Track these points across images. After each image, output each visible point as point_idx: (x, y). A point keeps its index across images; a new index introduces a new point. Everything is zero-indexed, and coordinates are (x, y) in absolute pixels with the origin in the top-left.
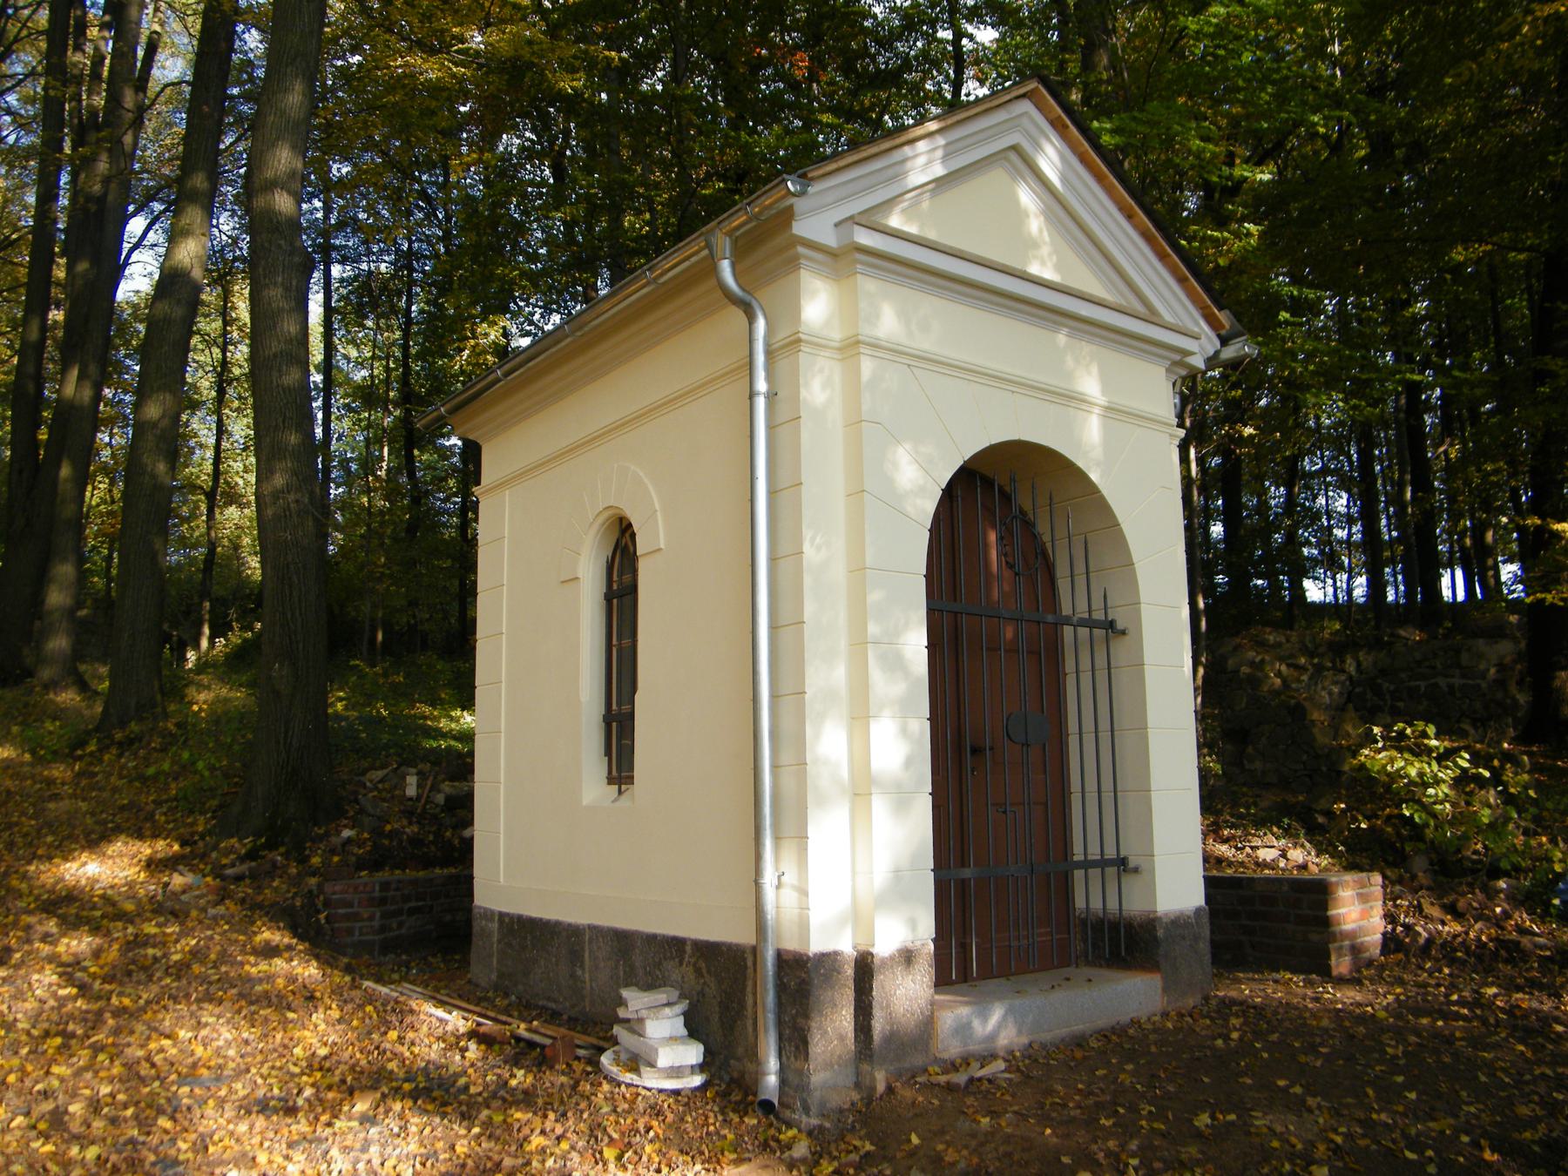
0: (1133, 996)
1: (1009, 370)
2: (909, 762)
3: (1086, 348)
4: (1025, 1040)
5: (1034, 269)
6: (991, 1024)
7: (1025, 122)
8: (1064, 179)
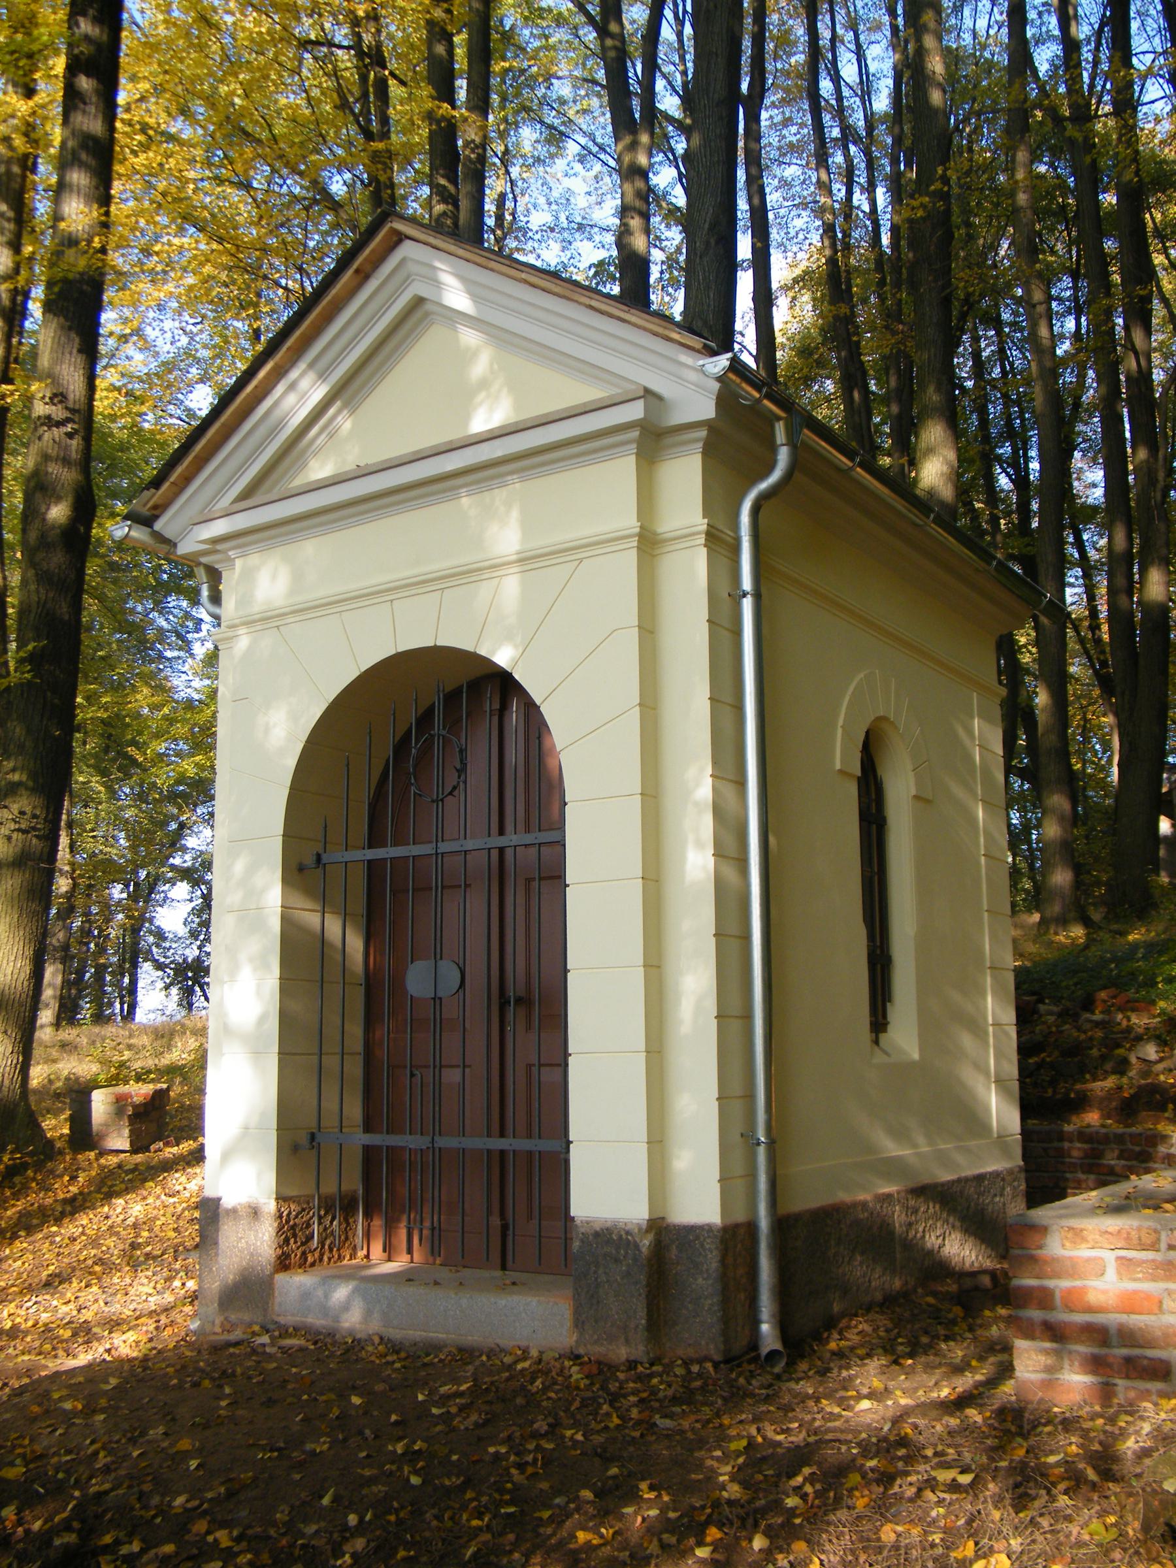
0: (530, 1319)
1: (373, 582)
2: (262, 1019)
3: (499, 495)
4: (375, 1326)
5: (482, 421)
6: (359, 1292)
7: (411, 267)
8: (474, 297)
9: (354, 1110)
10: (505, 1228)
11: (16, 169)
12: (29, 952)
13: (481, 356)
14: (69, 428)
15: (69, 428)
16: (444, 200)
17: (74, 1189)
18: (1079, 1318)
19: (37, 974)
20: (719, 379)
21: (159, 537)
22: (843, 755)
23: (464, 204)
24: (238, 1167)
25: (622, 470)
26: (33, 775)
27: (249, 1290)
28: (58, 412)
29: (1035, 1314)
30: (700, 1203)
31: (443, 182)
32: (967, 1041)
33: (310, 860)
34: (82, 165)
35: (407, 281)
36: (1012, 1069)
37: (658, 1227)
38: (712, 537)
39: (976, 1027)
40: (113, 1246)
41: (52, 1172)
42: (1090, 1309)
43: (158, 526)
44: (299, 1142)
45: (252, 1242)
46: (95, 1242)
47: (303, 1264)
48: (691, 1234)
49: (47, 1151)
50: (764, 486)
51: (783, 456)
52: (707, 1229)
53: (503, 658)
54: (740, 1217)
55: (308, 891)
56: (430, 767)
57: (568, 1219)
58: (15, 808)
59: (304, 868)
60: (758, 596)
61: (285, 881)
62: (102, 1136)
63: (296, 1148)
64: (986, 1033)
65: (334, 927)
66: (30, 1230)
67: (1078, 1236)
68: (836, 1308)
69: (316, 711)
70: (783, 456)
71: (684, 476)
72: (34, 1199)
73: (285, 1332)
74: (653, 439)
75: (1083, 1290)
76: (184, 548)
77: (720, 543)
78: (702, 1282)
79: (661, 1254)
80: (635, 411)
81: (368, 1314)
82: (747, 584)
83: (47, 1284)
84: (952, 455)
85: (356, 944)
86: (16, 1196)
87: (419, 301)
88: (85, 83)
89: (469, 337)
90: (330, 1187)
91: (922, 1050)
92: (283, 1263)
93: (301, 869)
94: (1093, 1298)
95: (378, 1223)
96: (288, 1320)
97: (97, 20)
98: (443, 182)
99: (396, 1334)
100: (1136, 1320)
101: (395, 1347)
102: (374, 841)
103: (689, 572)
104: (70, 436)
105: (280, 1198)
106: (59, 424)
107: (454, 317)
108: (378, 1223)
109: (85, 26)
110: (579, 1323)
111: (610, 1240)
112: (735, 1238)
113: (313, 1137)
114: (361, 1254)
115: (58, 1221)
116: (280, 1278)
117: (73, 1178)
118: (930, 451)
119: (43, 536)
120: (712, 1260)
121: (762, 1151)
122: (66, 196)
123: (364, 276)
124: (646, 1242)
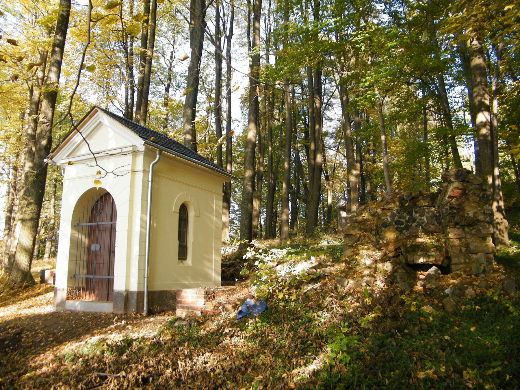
4: (82, 309)
9: (85, 272)
10: (108, 293)
11: (45, 53)
12: (32, 239)
13: (111, 134)
14: (47, 124)
15: (47, 124)
16: (143, 67)
17: (39, 291)
18: (185, 305)
19: (34, 244)
20: (144, 145)
21: (53, 162)
22: (175, 208)
23: (147, 69)
24: (62, 283)
25: (130, 157)
26: (35, 201)
27: (62, 304)
28: (45, 121)
29: (179, 305)
30: (134, 288)
31: (143, 63)
32: (207, 264)
33: (76, 225)
34: (55, 66)
35: (99, 118)
36: (220, 269)
37: (127, 292)
38: (144, 171)
39: (210, 261)
40: (44, 302)
41: (35, 287)
42: (188, 304)
43: (53, 159)
44: (72, 277)
45: (62, 294)
46: (41, 301)
47: (72, 299)
48: (133, 293)
49: (35, 283)
50: (154, 162)
51: (158, 156)
52: (135, 292)
53: (109, 191)
54: (142, 290)
55: (76, 230)
56: (97, 207)
57: (113, 290)
58: (31, 208)
59: (76, 226)
60: (152, 182)
61: (72, 228)
62: (47, 281)
63: (71, 278)
64: (212, 262)
65: (80, 236)
66: (28, 298)
67: (186, 292)
68: (165, 309)
69: (78, 197)
70: (158, 156)
71: (140, 159)
72: (31, 293)
73: (66, 310)
74: (135, 152)
75: (185, 301)
76: (57, 164)
77: (145, 171)
78: (133, 301)
79: (127, 296)
80: (131, 149)
81: (81, 307)
82: (150, 179)
83: (29, 307)
84: (255, 131)
85: (87, 241)
86: (26, 292)
87: (101, 122)
88: (57, 49)
89: (110, 130)
90: (77, 286)
91: (192, 264)
92: (68, 299)
93: (75, 226)
94: (187, 302)
95: (88, 292)
96: (68, 309)
97: (61, 36)
98: (143, 63)
99: (85, 311)
100: (192, 305)
101: (84, 313)
102: (91, 221)
103: (139, 176)
104: (47, 126)
105: (68, 287)
106: (45, 123)
107: (107, 126)
108: (88, 292)
109: (58, 37)
110: (114, 308)
111: (119, 293)
112: (140, 294)
113: (74, 276)
114: (84, 298)
115: (35, 297)
116: (67, 301)
117: (39, 289)
118: (250, 130)
119: (40, 148)
120: (135, 297)
121: (146, 279)
122: (50, 72)
123: (91, 117)
124: (125, 294)
